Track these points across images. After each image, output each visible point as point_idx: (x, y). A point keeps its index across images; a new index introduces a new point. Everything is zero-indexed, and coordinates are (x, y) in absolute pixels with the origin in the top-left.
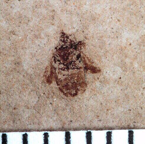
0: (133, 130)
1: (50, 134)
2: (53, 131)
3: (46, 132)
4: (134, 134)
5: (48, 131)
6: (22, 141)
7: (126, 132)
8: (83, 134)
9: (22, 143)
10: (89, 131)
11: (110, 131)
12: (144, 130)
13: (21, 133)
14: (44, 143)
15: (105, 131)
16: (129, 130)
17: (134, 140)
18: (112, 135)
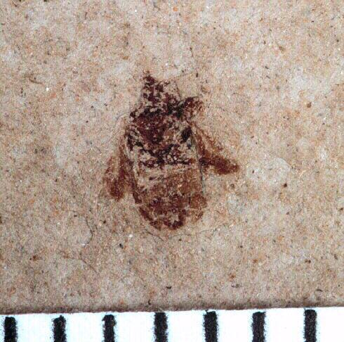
0: (316, 309)
1: (119, 317)
2: (127, 311)
3: (109, 313)
4: (319, 319)
5: (113, 311)
6: (51, 334)
7: (298, 315)
8: (196, 318)
9: (52, 340)
10: (210, 310)
11: (261, 311)
12: (342, 309)
13: (50, 315)
14: (105, 341)
15: (249, 310)
16: (307, 309)
17: (317, 334)
18: (266, 319)
